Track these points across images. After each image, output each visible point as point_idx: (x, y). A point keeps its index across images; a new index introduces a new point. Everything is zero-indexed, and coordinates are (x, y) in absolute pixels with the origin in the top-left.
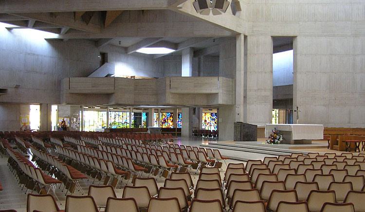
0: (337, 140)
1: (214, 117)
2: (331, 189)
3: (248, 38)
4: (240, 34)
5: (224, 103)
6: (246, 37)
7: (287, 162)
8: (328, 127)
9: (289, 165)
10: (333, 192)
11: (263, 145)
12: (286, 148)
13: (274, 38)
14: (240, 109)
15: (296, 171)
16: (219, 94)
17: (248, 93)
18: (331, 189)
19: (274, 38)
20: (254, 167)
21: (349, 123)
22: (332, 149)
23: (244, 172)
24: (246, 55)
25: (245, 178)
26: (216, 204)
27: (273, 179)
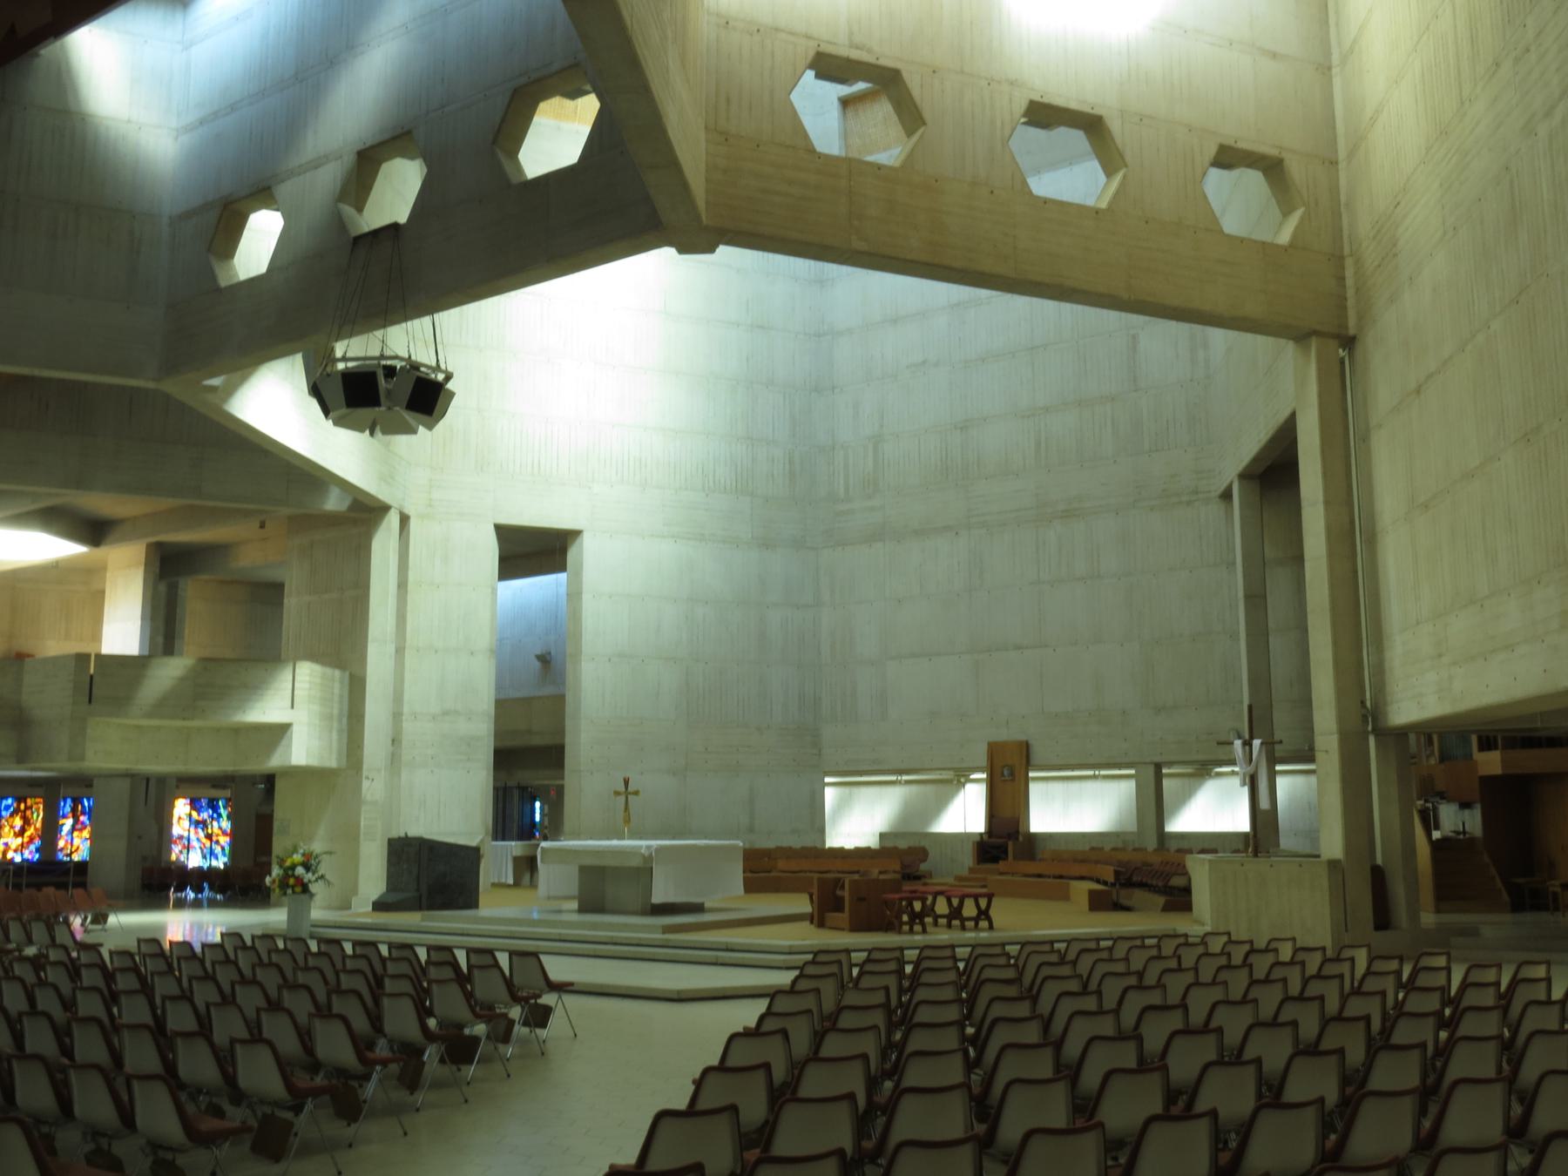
0: (839, 893)
1: (205, 815)
2: (1251, 996)
3: (414, 525)
4: (384, 509)
5: (313, 762)
6: (404, 520)
7: (1120, 952)
8: (410, 835)
9: (1127, 959)
10: (1255, 1001)
11: (569, 925)
12: (611, 927)
13: (506, 534)
14: (373, 787)
15: (1140, 975)
16: (295, 728)
17: (405, 725)
18: (1251, 996)
19: (506, 534)
20: (1046, 971)
21: (751, 830)
22: (821, 924)
23: (1085, 986)
24: (402, 585)
25: (1022, 1010)
26: (843, 1109)
27: (1090, 1003)
